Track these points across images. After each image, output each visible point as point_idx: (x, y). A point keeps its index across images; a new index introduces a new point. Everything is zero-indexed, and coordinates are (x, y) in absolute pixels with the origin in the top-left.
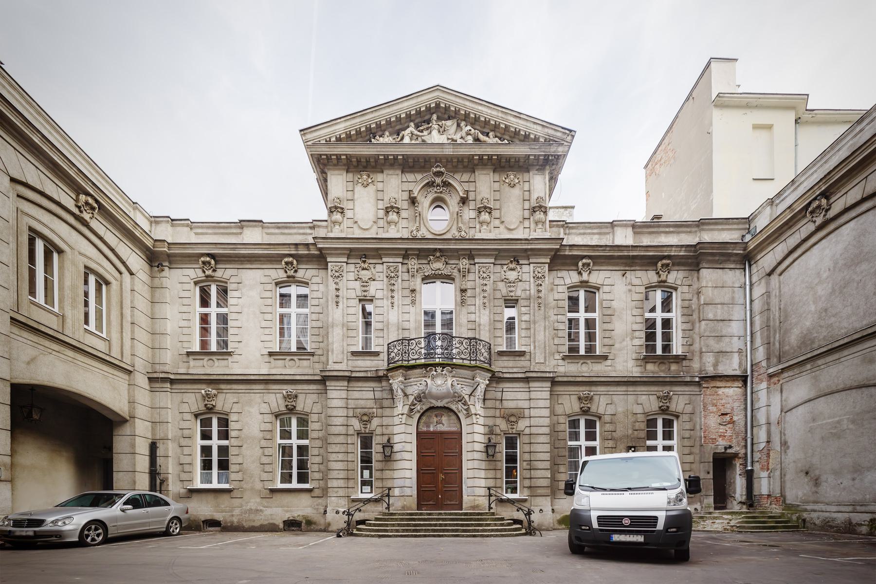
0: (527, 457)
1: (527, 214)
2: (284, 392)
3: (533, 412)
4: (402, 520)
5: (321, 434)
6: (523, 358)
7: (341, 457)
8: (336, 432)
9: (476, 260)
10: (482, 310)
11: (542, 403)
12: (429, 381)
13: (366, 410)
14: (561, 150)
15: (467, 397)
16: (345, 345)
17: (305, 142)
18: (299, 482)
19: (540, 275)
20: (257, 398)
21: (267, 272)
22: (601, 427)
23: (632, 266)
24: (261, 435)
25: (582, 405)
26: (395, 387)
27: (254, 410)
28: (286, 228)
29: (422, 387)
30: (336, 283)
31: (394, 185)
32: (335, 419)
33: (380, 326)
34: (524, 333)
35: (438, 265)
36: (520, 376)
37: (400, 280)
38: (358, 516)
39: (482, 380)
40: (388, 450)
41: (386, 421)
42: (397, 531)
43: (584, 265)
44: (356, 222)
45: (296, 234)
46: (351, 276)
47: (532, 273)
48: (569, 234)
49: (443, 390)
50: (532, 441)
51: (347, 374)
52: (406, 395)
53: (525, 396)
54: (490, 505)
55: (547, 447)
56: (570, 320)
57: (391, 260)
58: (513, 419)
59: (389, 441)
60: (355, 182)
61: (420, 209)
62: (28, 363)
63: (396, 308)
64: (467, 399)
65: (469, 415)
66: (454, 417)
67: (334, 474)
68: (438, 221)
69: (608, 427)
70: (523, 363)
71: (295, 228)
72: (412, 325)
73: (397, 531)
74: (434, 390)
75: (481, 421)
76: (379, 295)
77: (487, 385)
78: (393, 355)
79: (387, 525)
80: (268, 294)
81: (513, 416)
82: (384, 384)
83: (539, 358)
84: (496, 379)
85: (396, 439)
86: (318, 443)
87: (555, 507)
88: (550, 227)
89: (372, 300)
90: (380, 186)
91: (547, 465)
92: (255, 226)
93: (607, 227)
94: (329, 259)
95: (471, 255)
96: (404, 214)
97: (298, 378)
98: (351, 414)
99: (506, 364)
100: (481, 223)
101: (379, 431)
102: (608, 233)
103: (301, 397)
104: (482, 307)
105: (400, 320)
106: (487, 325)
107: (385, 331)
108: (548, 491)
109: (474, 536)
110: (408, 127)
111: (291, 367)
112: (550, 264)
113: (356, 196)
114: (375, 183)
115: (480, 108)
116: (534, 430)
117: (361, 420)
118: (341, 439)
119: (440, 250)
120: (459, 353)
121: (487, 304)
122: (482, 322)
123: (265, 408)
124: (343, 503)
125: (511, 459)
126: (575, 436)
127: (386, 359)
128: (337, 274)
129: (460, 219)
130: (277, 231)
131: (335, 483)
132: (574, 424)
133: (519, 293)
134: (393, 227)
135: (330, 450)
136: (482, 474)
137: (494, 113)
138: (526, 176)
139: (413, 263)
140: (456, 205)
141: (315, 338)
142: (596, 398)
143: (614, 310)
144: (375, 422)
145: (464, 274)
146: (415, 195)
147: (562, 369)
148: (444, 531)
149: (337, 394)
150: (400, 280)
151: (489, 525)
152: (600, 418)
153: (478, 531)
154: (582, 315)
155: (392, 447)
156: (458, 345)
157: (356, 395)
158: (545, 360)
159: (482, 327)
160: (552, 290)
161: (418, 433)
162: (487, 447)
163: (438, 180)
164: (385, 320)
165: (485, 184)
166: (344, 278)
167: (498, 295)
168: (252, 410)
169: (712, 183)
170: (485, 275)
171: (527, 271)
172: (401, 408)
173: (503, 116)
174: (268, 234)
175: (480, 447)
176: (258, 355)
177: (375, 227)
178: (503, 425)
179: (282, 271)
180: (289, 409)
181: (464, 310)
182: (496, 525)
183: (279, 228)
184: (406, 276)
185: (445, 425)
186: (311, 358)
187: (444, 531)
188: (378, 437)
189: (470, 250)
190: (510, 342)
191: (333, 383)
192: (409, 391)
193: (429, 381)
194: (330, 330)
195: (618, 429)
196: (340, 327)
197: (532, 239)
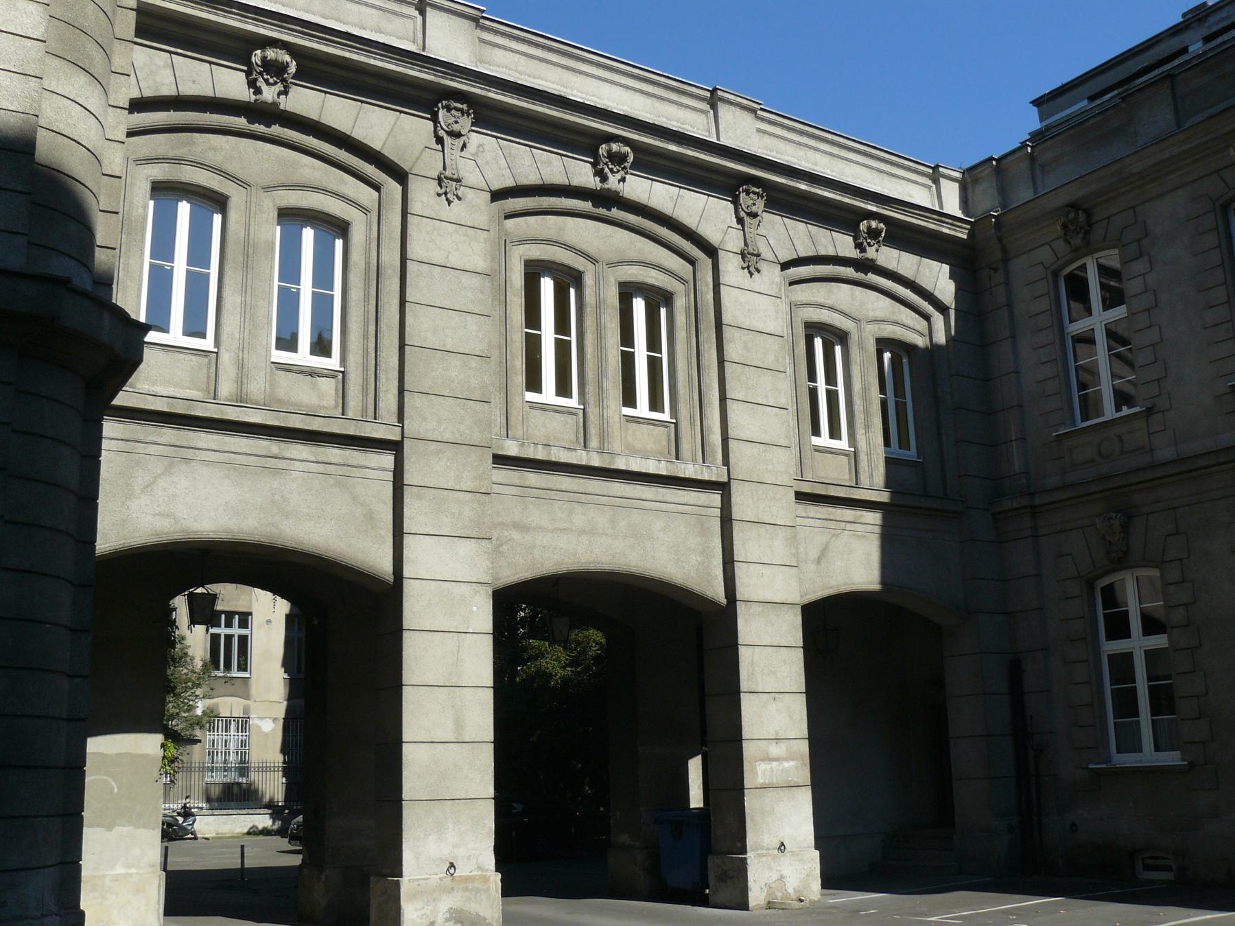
62: (819, 561)
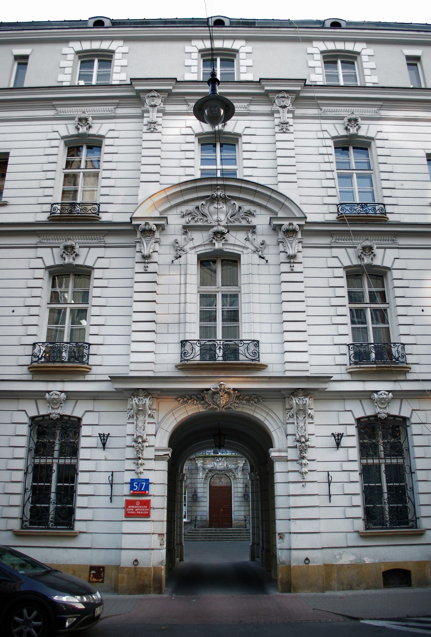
4: (203, 533)
15: (234, 470)
26: (199, 465)
40: (195, 496)
42: (201, 538)
49: (222, 467)
52: (204, 469)
54: (245, 525)
59: (195, 492)
65: (235, 478)
66: (228, 478)
73: (201, 538)
74: (218, 467)
79: (196, 535)
82: (193, 462)
85: (199, 490)
101: (190, 486)
109: (236, 540)
136: (242, 509)
151: (243, 535)
153: (238, 538)
155: (197, 495)
161: (211, 487)
162: (244, 495)
169: (339, 391)
172: (201, 475)
175: (240, 495)
185: (223, 482)
193: (215, 464)
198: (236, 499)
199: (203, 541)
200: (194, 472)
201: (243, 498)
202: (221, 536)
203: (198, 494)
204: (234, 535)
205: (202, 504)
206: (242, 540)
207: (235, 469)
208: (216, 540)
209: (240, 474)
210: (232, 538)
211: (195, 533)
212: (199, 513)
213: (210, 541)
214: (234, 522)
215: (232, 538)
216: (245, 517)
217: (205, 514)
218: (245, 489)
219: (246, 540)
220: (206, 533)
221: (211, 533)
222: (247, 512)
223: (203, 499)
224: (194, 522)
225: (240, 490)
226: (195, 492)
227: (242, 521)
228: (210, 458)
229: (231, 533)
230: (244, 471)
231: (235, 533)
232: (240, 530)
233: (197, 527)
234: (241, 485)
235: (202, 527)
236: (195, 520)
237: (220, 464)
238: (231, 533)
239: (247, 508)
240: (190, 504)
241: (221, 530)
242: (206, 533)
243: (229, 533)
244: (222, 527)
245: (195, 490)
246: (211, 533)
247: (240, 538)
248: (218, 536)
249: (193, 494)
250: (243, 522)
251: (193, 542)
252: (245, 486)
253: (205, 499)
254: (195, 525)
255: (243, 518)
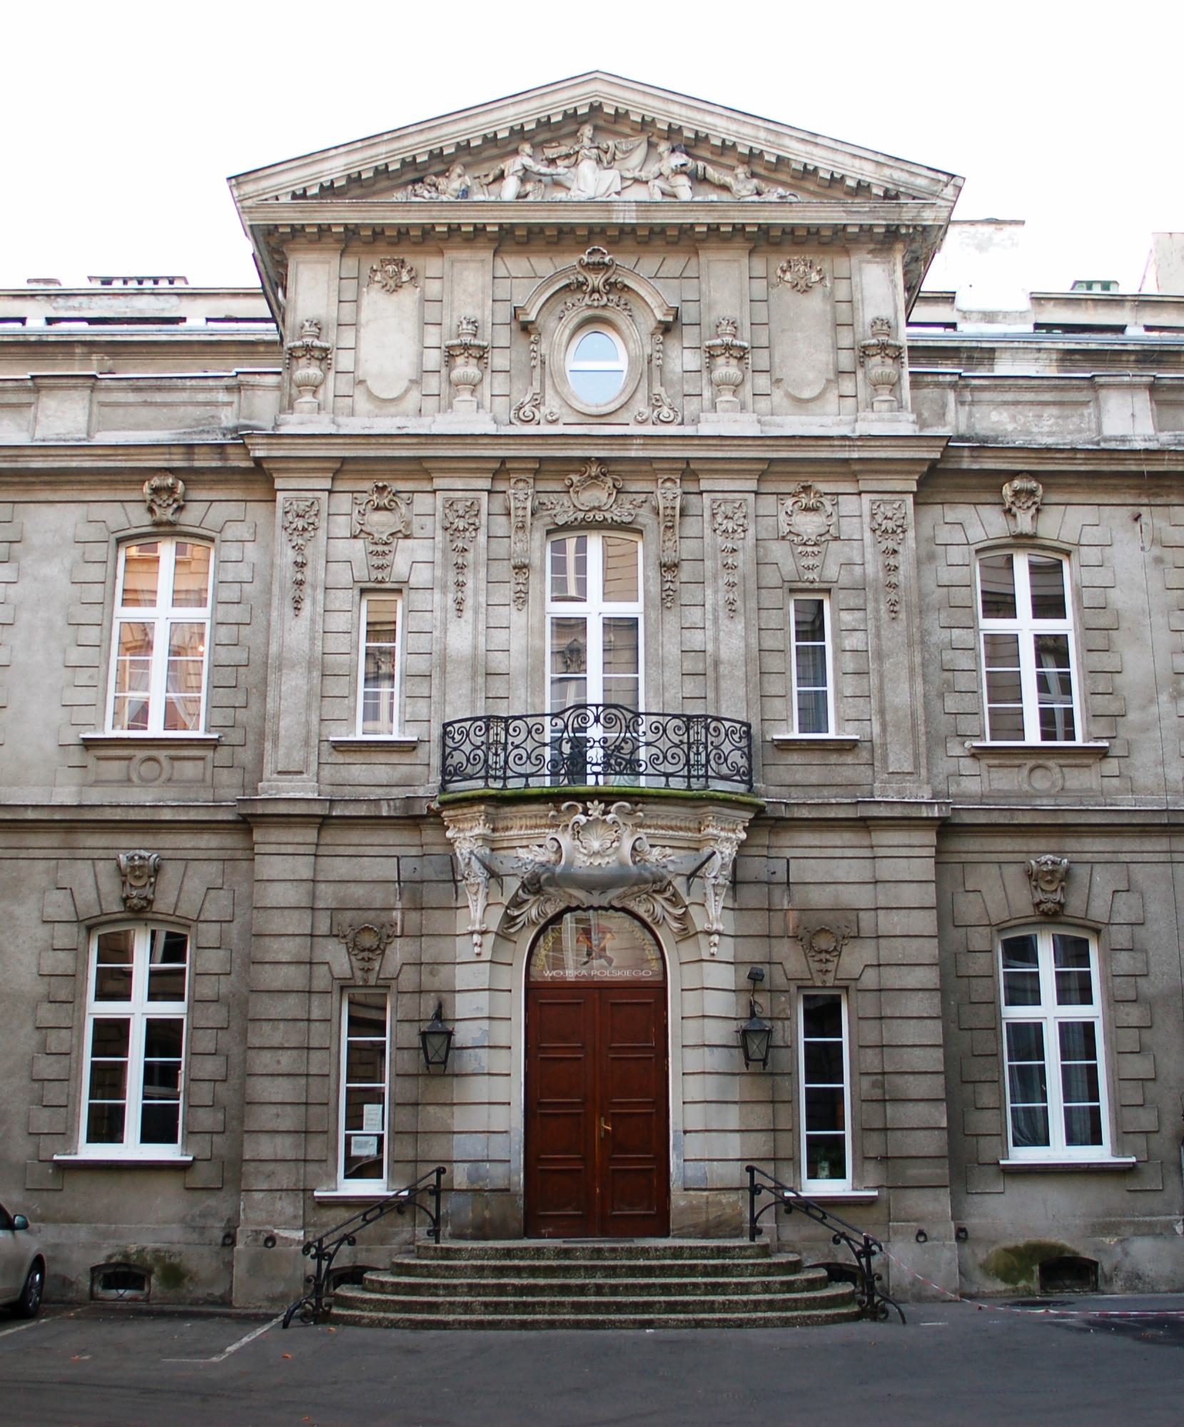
0: (871, 1060)
1: (846, 360)
2: (123, 858)
3: (890, 923)
4: (480, 1271)
5: (225, 986)
6: (849, 759)
7: (286, 1061)
8: (277, 985)
9: (704, 485)
10: (724, 623)
11: (911, 895)
12: (566, 840)
13: (371, 915)
14: (928, 217)
15: (679, 883)
16: (315, 720)
17: (239, 201)
18: (147, 1137)
19: (890, 525)
20: (38, 872)
21: (98, 511)
22: (1104, 961)
23: (1157, 495)
24: (41, 988)
25: (1039, 896)
26: (464, 849)
27: (26, 912)
28: (159, 389)
29: (543, 856)
30: (298, 549)
31: (472, 289)
32: (275, 944)
33: (421, 664)
34: (849, 688)
35: (597, 496)
36: (841, 813)
37: (482, 538)
38: (344, 1257)
39: (725, 839)
40: (436, 1041)
41: (430, 949)
42: (467, 1308)
43: (1017, 493)
44: (362, 382)
45: (184, 404)
46: (341, 526)
47: (867, 519)
48: (973, 403)
49: (607, 863)
50: (888, 1012)
51: (318, 810)
52: (494, 875)
53: (858, 870)
54: (754, 1220)
55: (933, 1033)
56: (992, 640)
57: (459, 484)
58: (824, 942)
59: (439, 1016)
60: (365, 280)
61: (544, 348)
63: (468, 614)
64: (682, 891)
65: (686, 933)
67: (265, 1119)
68: (595, 374)
69: (1125, 962)
70: (848, 770)
71: (184, 389)
72: (515, 662)
73: (467, 1308)
74: (582, 863)
75: (726, 949)
76: (421, 576)
77: (742, 845)
78: (458, 758)
80: (95, 572)
81: (825, 933)
82: (429, 835)
83: (899, 759)
84: (765, 822)
85: (463, 1006)
86: (215, 1016)
87: (971, 1223)
88: (915, 385)
89: (400, 591)
90: (433, 288)
91: (935, 1086)
92: (75, 387)
93: (1079, 389)
94: (279, 484)
95: (688, 471)
96: (499, 360)
97: (167, 815)
98: (323, 927)
99: (800, 776)
100: (717, 385)
101: (408, 979)
102: (1086, 404)
103: (171, 872)
104: (722, 614)
105: (482, 647)
106: (741, 663)
107: (436, 681)
108: (941, 1172)
110: (516, 152)
111: (146, 782)
112: (915, 494)
113: (364, 316)
114: (421, 281)
115: (709, 119)
116: (893, 978)
117: (354, 947)
118: (291, 1007)
119: (600, 460)
120: (653, 760)
121: (739, 604)
122: (725, 654)
123: (58, 905)
124: (290, 1210)
125: (824, 1063)
126: (1025, 991)
127: (436, 761)
128: (300, 523)
129: (656, 374)
130: (132, 397)
131: (266, 1148)
132: (1021, 950)
133: (832, 572)
134: (466, 396)
135: (254, 1041)
136: (733, 1118)
137: (746, 130)
138: (842, 264)
139: (520, 494)
140: (647, 339)
141: (223, 697)
142: (1081, 872)
143: (1118, 614)
144: (399, 952)
145: (673, 521)
146: (532, 317)
147: (972, 786)
148: (607, 1308)
149: (283, 867)
150: (482, 538)
151: (745, 1289)
152: (1098, 932)
154: (1026, 626)
155: (450, 1034)
156: (651, 737)
157: (341, 868)
158: (917, 765)
159: (723, 669)
160: (931, 557)
161: (532, 989)
162: (744, 1033)
163: (596, 280)
164: (436, 648)
165: (725, 285)
166: (321, 534)
167: (771, 578)
168: (19, 911)
170: (730, 525)
171: (855, 510)
172: (478, 911)
173: (772, 138)
174: (103, 404)
175: (720, 1032)
176: (50, 745)
177: (415, 395)
178: (792, 960)
179: (141, 508)
180: (131, 909)
181: (672, 621)
182: (767, 1288)
183: (138, 389)
184: (501, 525)
185: (615, 958)
186: (209, 754)
187: (607, 1308)
188: (405, 999)
189: (688, 460)
190: (813, 712)
191: (276, 835)
192: (505, 862)
193: (566, 840)
194: (272, 678)
195: (1154, 969)
196: (301, 670)
197: (861, 438)
198: (695, 1060)
199: (480, 1325)
200: (433, 895)
201: (738, 1053)
202: (599, 1290)
203: (459, 1027)
204: (682, 1289)
205: (479, 1089)
206: (740, 1324)
207: (691, 876)
208: (564, 1325)
209: (715, 907)
210: (671, 1307)
211: (430, 1272)
212: (464, 1147)
213: (523, 1325)
214: (678, 1199)
215: (671, 1307)
216: (750, 1170)
217: (498, 1148)
218: (744, 998)
219: (767, 1323)
220: (501, 1272)
221: (534, 1272)
222: (761, 1137)
223: (485, 1059)
224: (430, 1203)
225: (719, 1004)
226: (439, 1016)
227: (733, 1197)
228: (535, 808)
229: (665, 1271)
230: (745, 891)
231: (693, 1270)
232: (721, 1252)
233: (447, 1230)
234: (725, 976)
235: (481, 1232)
236: (437, 1191)
237: (596, 845)
238: (665, 1271)
239: (760, 1116)
240: (409, 1090)
241: (598, 1253)
242: (501, 1272)
243: (649, 1271)
244: (604, 1233)
245: (440, 1006)
246: (534, 1272)
247: (727, 1307)
248: (582, 1290)
249: (425, 1027)
250: (738, 1202)
251: (409, 1336)
252: (745, 983)
253: (499, 1061)
254: (436, 1221)
255: (734, 1174)
